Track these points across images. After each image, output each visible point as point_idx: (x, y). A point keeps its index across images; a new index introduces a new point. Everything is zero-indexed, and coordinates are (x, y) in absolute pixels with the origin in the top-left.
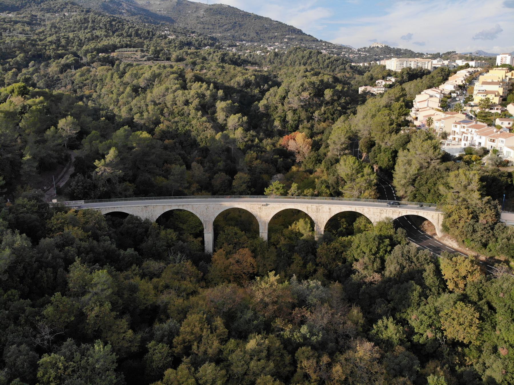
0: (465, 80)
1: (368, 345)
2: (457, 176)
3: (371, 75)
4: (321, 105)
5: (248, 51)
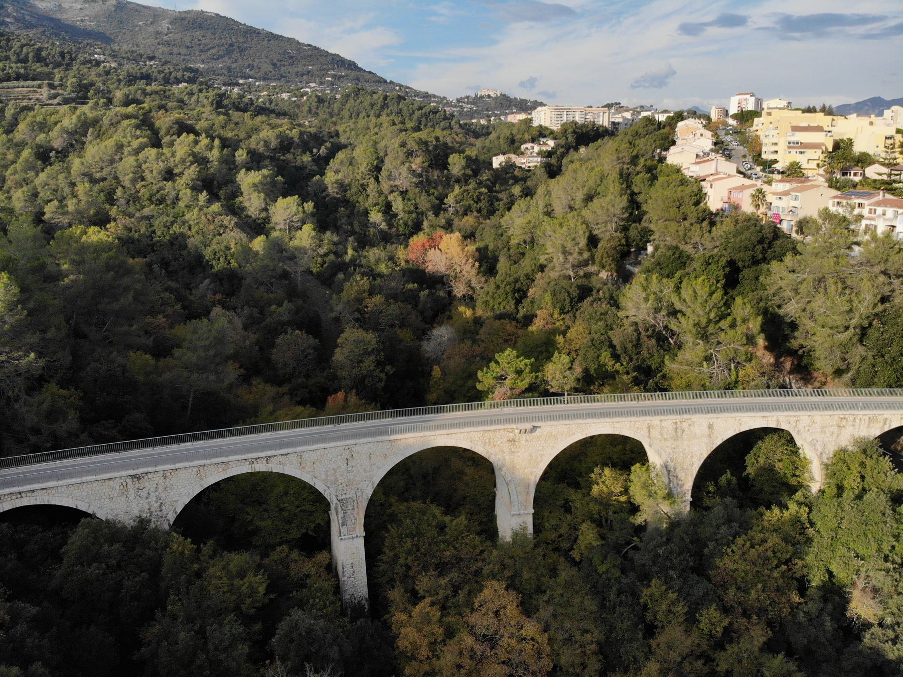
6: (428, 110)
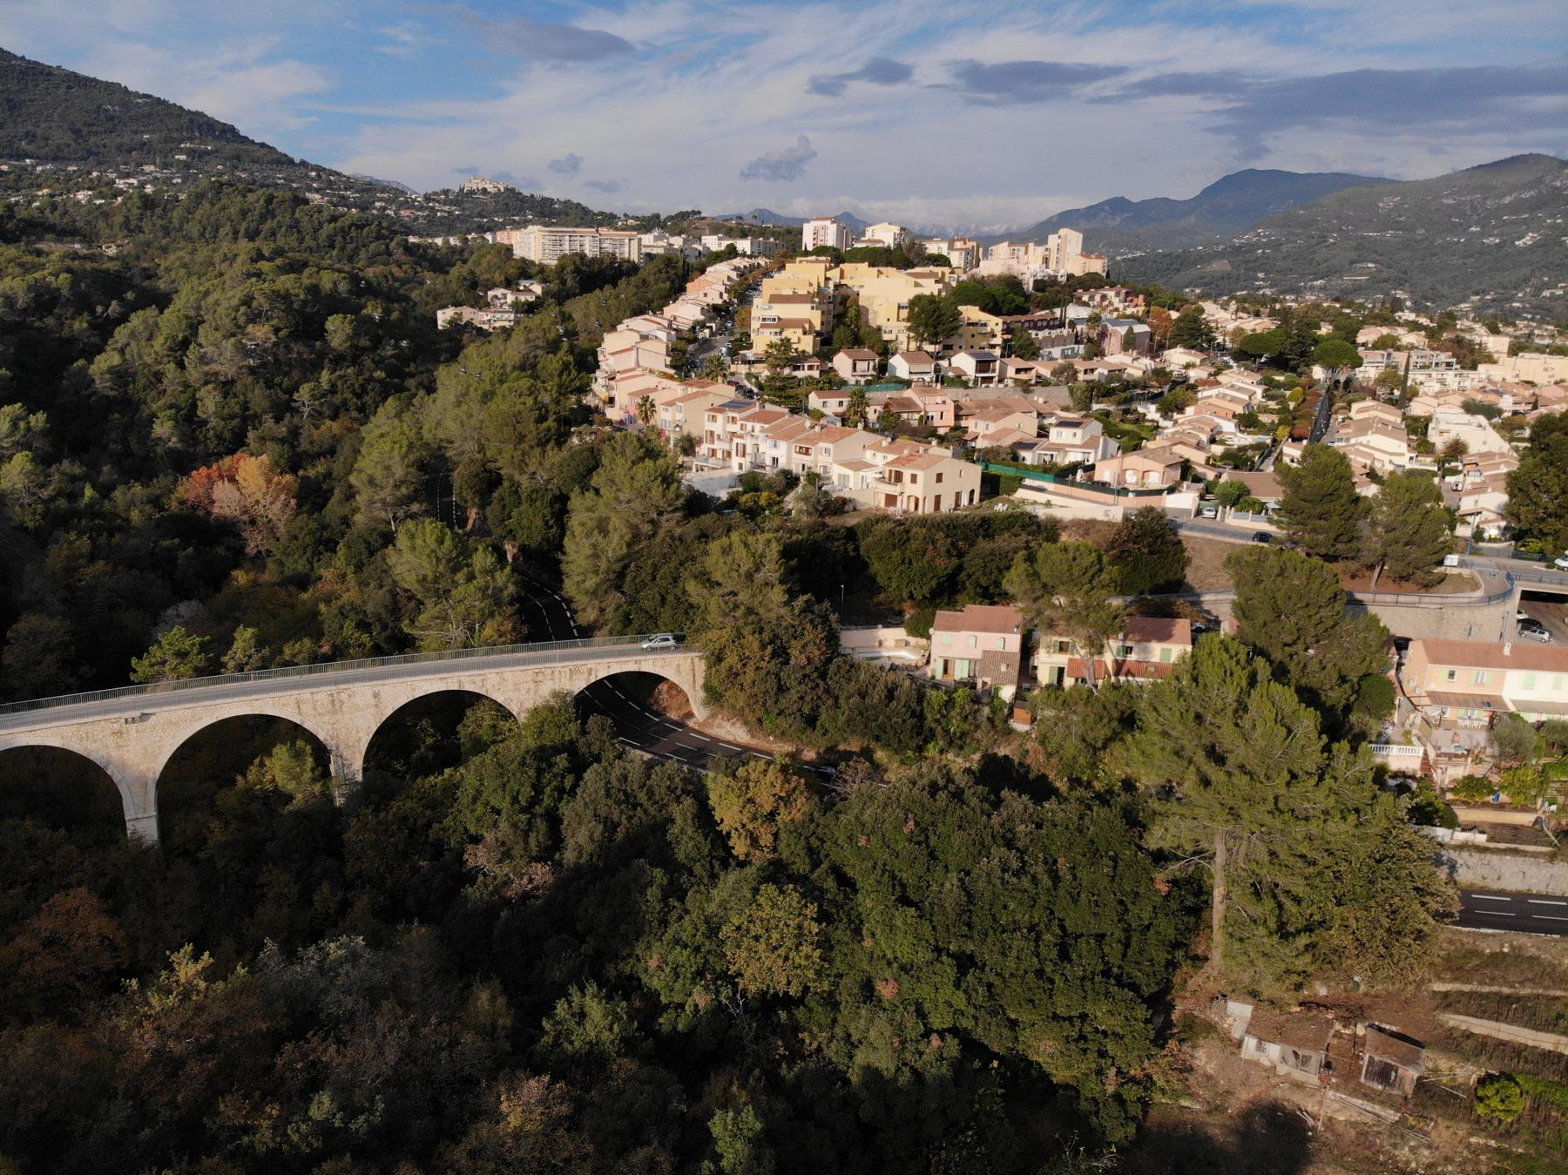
0: (727, 291)
1: (533, 1087)
2: (726, 551)
3: (472, 273)
4: (316, 367)
5: (45, 191)
6: (348, 223)
